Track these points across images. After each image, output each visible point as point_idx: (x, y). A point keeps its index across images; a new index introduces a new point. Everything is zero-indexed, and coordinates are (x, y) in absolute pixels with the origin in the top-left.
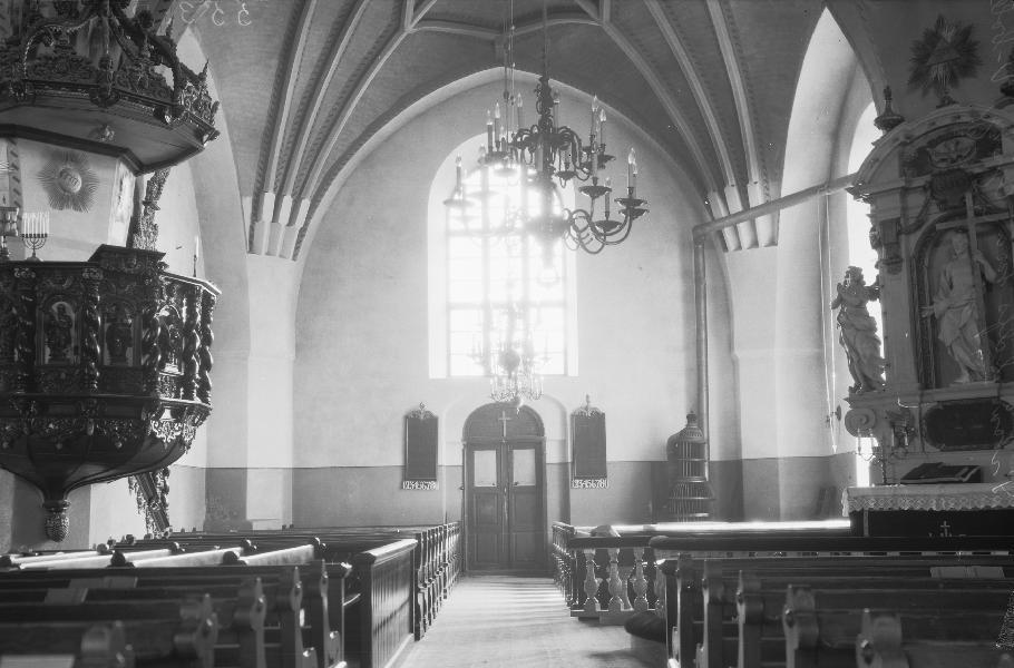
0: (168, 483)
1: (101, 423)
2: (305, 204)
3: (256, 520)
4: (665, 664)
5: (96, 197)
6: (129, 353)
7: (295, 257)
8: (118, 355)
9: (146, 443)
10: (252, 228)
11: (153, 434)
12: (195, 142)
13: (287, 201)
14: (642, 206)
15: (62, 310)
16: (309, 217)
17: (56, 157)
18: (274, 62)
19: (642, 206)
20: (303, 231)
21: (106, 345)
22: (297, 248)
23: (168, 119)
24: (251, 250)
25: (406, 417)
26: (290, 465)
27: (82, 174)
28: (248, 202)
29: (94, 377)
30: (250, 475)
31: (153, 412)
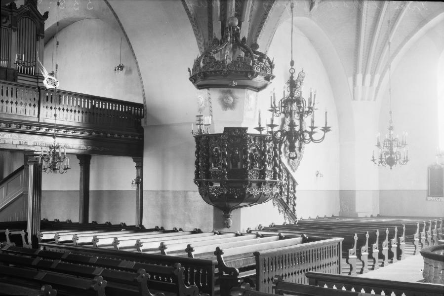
0: (296, 202)
1: (229, 189)
2: (377, 77)
3: (360, 212)
4: (390, 295)
5: (238, 105)
6: (239, 164)
7: (375, 100)
8: (235, 165)
9: (247, 196)
10: (354, 90)
11: (249, 193)
12: (266, 82)
13: (368, 76)
14: (330, 129)
15: (217, 150)
16: (380, 82)
17: (223, 92)
18: (355, 20)
19: (330, 129)
20: (378, 89)
21: (230, 162)
22: (376, 95)
23: (249, 76)
24: (354, 99)
25: (428, 168)
26: (377, 189)
27: (233, 97)
28: (351, 79)
29: (225, 174)
30: (357, 194)
31: (247, 185)
